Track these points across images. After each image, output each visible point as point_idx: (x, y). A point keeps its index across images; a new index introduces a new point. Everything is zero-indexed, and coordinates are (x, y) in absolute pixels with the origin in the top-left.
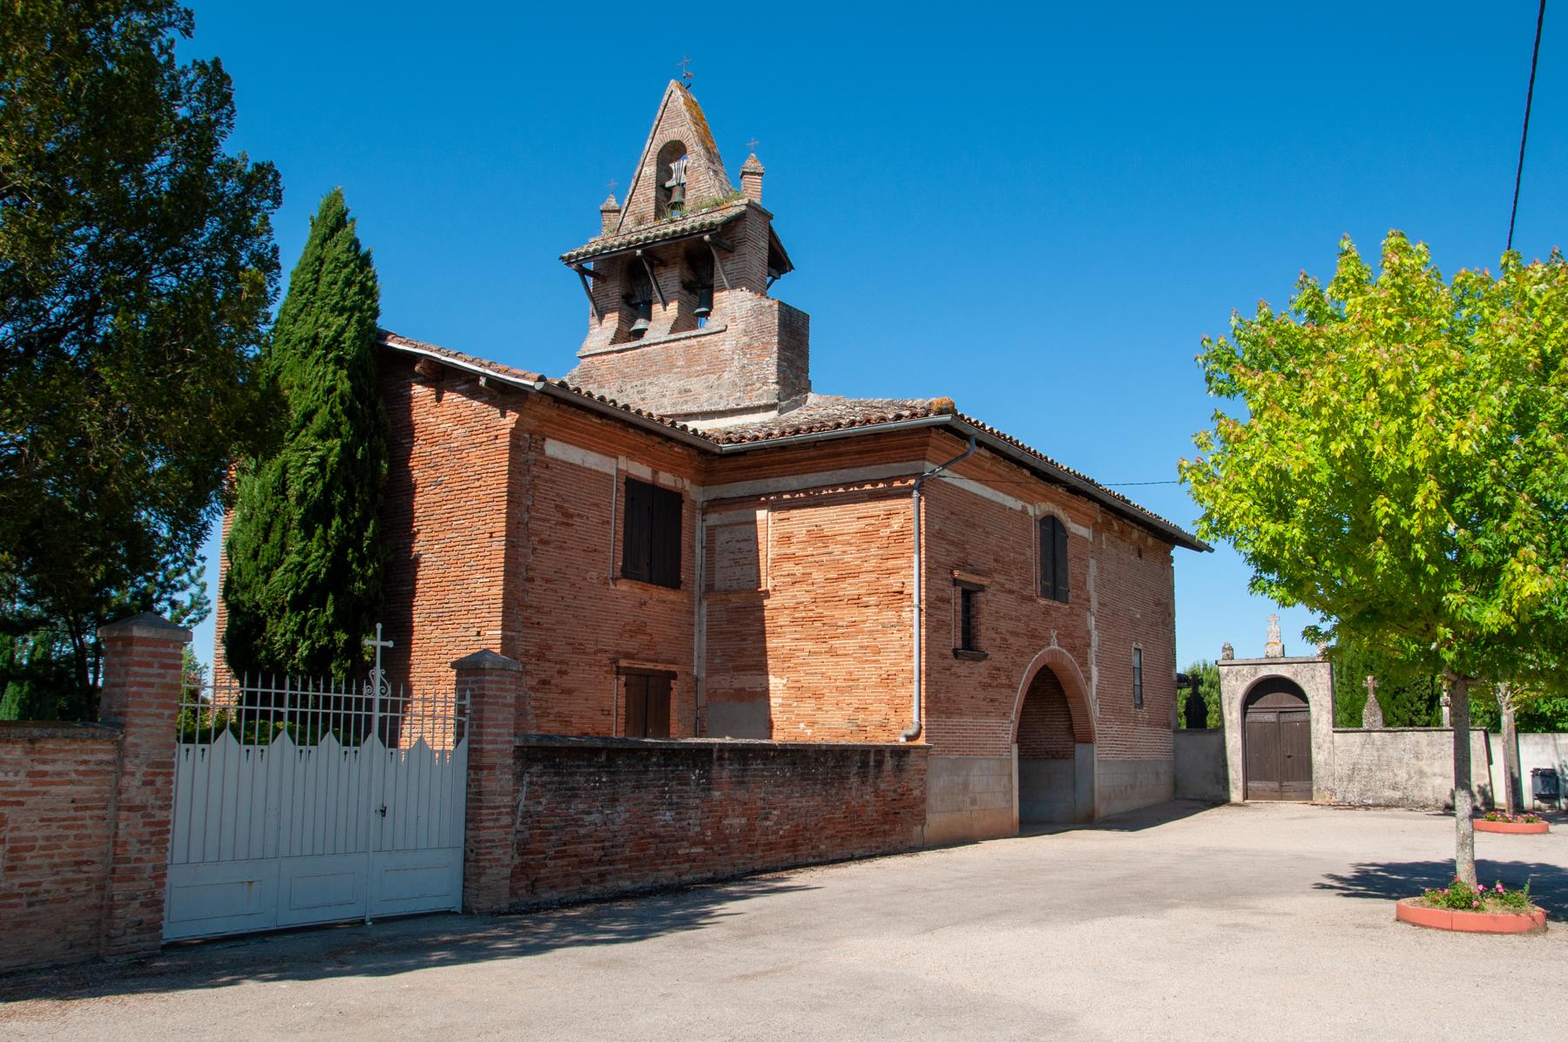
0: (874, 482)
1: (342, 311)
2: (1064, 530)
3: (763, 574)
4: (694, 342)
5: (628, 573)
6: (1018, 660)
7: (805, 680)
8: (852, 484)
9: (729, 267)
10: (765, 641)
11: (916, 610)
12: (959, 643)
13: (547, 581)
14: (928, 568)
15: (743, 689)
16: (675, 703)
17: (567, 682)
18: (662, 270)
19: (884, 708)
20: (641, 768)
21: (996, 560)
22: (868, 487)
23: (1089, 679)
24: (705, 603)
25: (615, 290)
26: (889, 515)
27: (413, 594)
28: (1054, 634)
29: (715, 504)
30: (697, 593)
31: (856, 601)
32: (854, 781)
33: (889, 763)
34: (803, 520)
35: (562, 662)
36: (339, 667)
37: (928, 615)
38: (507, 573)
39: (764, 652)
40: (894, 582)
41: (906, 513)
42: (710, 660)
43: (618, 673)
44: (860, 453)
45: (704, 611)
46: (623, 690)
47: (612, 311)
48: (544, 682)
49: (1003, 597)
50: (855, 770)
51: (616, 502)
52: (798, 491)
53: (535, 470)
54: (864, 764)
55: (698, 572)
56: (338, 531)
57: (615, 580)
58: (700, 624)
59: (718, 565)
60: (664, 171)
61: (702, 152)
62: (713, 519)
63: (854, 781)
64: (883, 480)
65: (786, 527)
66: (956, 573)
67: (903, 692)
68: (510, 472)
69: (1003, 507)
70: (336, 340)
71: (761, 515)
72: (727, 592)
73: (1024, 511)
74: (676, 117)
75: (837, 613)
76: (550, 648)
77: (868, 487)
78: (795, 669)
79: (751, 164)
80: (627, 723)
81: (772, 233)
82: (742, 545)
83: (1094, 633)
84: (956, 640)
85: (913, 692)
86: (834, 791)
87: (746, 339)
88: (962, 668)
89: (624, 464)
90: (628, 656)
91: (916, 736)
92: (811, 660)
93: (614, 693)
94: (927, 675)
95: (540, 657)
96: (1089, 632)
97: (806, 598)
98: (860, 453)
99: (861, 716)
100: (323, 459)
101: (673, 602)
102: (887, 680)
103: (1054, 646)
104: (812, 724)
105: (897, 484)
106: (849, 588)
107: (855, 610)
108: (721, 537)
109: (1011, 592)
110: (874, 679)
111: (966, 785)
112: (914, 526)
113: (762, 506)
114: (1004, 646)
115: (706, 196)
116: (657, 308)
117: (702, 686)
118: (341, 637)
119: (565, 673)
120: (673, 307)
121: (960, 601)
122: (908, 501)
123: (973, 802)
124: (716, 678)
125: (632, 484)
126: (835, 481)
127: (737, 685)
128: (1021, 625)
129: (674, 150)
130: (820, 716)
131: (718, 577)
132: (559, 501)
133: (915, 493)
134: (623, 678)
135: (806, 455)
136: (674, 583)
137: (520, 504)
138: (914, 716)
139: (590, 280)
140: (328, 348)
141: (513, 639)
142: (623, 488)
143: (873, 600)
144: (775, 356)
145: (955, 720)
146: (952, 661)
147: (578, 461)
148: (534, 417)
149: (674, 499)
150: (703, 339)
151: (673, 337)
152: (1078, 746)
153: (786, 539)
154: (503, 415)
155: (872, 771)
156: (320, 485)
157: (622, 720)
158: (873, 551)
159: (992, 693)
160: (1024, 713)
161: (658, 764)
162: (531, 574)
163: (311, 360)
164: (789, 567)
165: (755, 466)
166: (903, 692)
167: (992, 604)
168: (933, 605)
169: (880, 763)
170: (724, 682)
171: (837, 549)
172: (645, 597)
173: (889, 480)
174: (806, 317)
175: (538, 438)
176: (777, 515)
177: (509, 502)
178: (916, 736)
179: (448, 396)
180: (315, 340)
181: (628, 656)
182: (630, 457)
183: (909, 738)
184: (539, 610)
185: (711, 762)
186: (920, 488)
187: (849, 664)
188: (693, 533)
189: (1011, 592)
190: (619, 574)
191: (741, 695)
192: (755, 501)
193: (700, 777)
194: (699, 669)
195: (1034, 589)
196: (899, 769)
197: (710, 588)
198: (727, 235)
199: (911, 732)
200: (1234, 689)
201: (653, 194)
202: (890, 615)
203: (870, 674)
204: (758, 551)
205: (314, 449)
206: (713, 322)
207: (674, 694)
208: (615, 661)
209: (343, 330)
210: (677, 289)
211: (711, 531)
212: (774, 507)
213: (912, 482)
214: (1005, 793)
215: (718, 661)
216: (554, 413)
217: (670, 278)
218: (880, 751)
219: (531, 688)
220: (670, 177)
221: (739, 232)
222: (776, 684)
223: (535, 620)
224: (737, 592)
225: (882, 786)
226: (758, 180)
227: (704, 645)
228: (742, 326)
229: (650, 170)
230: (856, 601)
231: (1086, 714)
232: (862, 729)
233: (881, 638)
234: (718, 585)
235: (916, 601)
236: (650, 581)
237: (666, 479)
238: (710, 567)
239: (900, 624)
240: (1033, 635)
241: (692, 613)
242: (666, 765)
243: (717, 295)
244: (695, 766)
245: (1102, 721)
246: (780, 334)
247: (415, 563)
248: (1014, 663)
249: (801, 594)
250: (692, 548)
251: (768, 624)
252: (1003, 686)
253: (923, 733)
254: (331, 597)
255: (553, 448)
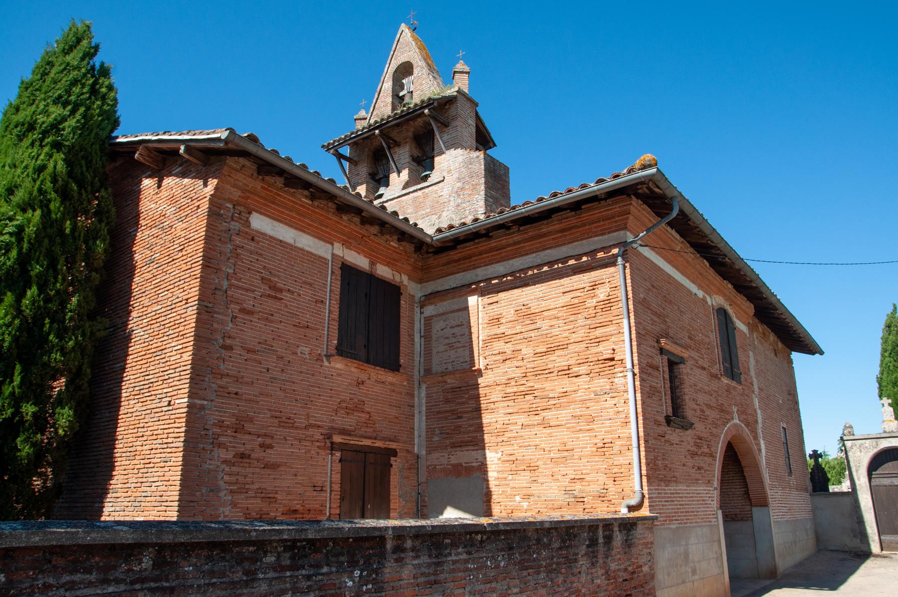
0: (578, 257)
1: (65, 104)
2: (732, 323)
3: (476, 355)
4: (420, 193)
5: (344, 350)
6: (714, 431)
7: (519, 453)
8: (557, 261)
9: (446, 137)
10: (481, 418)
11: (630, 375)
12: (670, 412)
13: (249, 351)
14: (638, 333)
15: (461, 465)
16: (395, 479)
17: (271, 456)
18: (396, 149)
19: (602, 478)
20: (239, 576)
21: (690, 338)
22: (572, 262)
23: (760, 450)
24: (424, 387)
25: (364, 170)
26: (594, 286)
27: (123, 369)
28: (735, 409)
29: (431, 298)
30: (416, 377)
31: (566, 372)
32: (583, 563)
33: (618, 538)
34: (511, 301)
35: (266, 435)
36: (26, 441)
37: (642, 380)
38: (198, 338)
39: (480, 428)
40: (605, 350)
41: (613, 281)
42: (429, 438)
43: (332, 449)
44: (563, 231)
45: (423, 394)
46: (338, 467)
47: (361, 184)
48: (243, 456)
49: (698, 371)
50: (583, 549)
51: (331, 285)
52: (504, 276)
53: (238, 240)
54: (593, 542)
55: (417, 359)
56: (33, 302)
57: (328, 357)
58: (420, 406)
59: (434, 351)
60: (398, 84)
61: (424, 64)
62: (430, 310)
63: (583, 563)
64: (585, 254)
65: (495, 310)
66: (663, 341)
67: (621, 460)
68: (208, 239)
69: (690, 292)
70: (56, 126)
71: (473, 300)
72: (444, 374)
73: (704, 300)
74: (406, 47)
75: (547, 385)
76: (251, 420)
77: (572, 262)
78: (508, 442)
79: (460, 66)
80: (342, 499)
81: (477, 113)
82: (456, 330)
83: (759, 412)
84: (666, 408)
85: (632, 460)
86: (560, 579)
87: (459, 185)
88: (674, 435)
89: (339, 250)
90: (343, 432)
91: (639, 506)
92: (524, 433)
93: (329, 469)
94: (646, 441)
95: (238, 429)
96: (755, 411)
97: (518, 373)
98: (563, 231)
99: (578, 486)
100: (21, 229)
101: (391, 384)
102: (604, 448)
103: (736, 421)
104: (527, 497)
105: (600, 255)
106: (558, 360)
107: (566, 381)
108: (437, 326)
109: (703, 368)
110: (590, 449)
111: (686, 555)
112: (621, 294)
113: (473, 292)
114: (703, 418)
115: (423, 87)
116: (393, 176)
117: (423, 464)
118: (29, 409)
119: (270, 447)
120: (405, 174)
121: (666, 369)
122: (612, 270)
123: (694, 572)
124: (435, 455)
125: (348, 271)
126: (539, 262)
127: (454, 460)
128: (714, 400)
129: (406, 69)
130: (535, 489)
131: (435, 360)
132: (265, 274)
133: (620, 259)
134: (338, 454)
135: (511, 241)
136: (394, 366)
137: (218, 270)
138: (635, 485)
139: (346, 164)
140: (45, 133)
141: (202, 407)
142: (338, 272)
143: (583, 369)
144: (483, 193)
145: (672, 488)
146: (664, 428)
147: (290, 241)
148: (235, 186)
149: (393, 291)
150: (426, 190)
151: (404, 192)
152: (755, 509)
153: (496, 321)
154: (205, 185)
155: (601, 549)
156: (14, 253)
157: (336, 496)
158: (581, 322)
159: (698, 461)
160: (723, 482)
161: (278, 567)
162: (228, 342)
163: (27, 142)
164: (499, 346)
165: (465, 258)
166: (621, 460)
167: (691, 375)
168: (645, 371)
169: (609, 539)
170: (443, 459)
171: (544, 325)
172: (363, 377)
173: (592, 253)
174: (507, 169)
175: (244, 210)
176: (486, 300)
177: (205, 267)
178: (639, 506)
179: (168, 181)
180: (31, 127)
181: (343, 432)
182: (346, 244)
183: (631, 508)
184: (237, 380)
185: (382, 555)
186: (624, 255)
187: (562, 435)
188: (412, 323)
189: (703, 368)
190: (334, 352)
191: (458, 470)
192: (468, 289)
193: (363, 581)
194: (419, 447)
195: (717, 369)
196: (628, 544)
197: (428, 371)
198: (441, 109)
199: (633, 502)
200: (861, 459)
201: (390, 100)
202: (602, 383)
203: (585, 443)
204: (471, 333)
205: (11, 219)
206: (435, 177)
207: (394, 470)
208: (329, 437)
209: (64, 119)
210: (407, 160)
211: (428, 321)
212: (483, 293)
213: (615, 251)
214: (717, 559)
215: (436, 438)
216: (257, 184)
217: (403, 154)
218: (607, 524)
219: (225, 462)
220: (403, 89)
221: (452, 111)
222: (493, 457)
223: (233, 389)
224: (451, 373)
225: (613, 566)
226: (466, 76)
227: (424, 424)
228: (456, 175)
229: (388, 85)
230: (566, 372)
231: (761, 482)
232: (580, 500)
233: (594, 408)
234: (435, 368)
235: (629, 365)
236: (368, 361)
237: (383, 271)
238: (428, 352)
239: (613, 392)
240: (722, 410)
241: (412, 396)
242: (293, 568)
243: (437, 159)
244: (353, 564)
245: (772, 487)
246: (485, 177)
247: (128, 338)
248: (712, 434)
249: (511, 370)
250: (411, 336)
251: (483, 401)
252: (704, 455)
253: (646, 503)
254: (18, 368)
255: (259, 222)
